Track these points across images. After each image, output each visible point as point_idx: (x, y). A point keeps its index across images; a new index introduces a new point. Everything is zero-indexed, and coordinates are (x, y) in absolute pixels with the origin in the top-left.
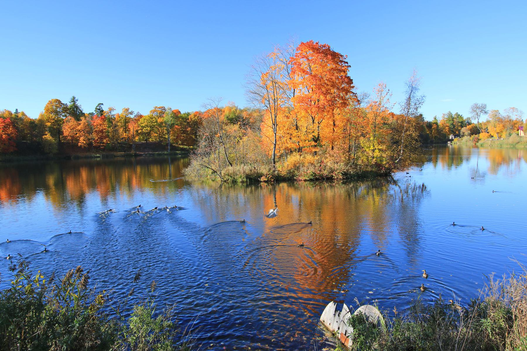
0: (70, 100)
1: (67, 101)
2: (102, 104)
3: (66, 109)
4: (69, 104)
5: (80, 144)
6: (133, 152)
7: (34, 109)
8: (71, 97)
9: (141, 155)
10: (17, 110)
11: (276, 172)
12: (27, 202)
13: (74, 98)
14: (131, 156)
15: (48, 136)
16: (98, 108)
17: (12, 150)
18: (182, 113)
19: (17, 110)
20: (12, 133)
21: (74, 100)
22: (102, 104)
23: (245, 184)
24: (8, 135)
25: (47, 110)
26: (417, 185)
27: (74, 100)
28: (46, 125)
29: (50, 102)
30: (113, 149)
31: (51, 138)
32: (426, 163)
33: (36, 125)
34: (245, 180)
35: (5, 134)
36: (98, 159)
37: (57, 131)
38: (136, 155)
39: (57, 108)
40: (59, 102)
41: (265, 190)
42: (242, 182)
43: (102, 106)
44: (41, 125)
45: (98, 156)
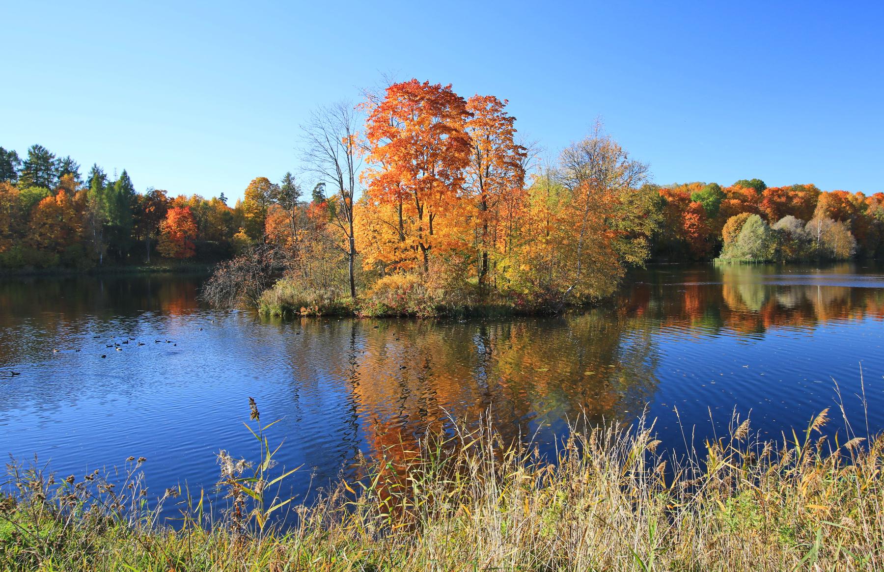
1: (277, 180)
2: (324, 184)
3: (275, 193)
7: (209, 195)
8: (285, 174)
10: (222, 194)
12: (859, 313)
13: (289, 175)
17: (188, 255)
18: (188, 197)
19: (222, 194)
20: (190, 230)
21: (289, 179)
22: (324, 184)
23: (279, 320)
24: (185, 232)
25: (248, 194)
27: (289, 179)
29: (254, 182)
32: (760, 276)
33: (232, 218)
35: (180, 231)
37: (257, 228)
39: (261, 190)
40: (265, 180)
42: (277, 315)
43: (324, 187)
44: (238, 217)
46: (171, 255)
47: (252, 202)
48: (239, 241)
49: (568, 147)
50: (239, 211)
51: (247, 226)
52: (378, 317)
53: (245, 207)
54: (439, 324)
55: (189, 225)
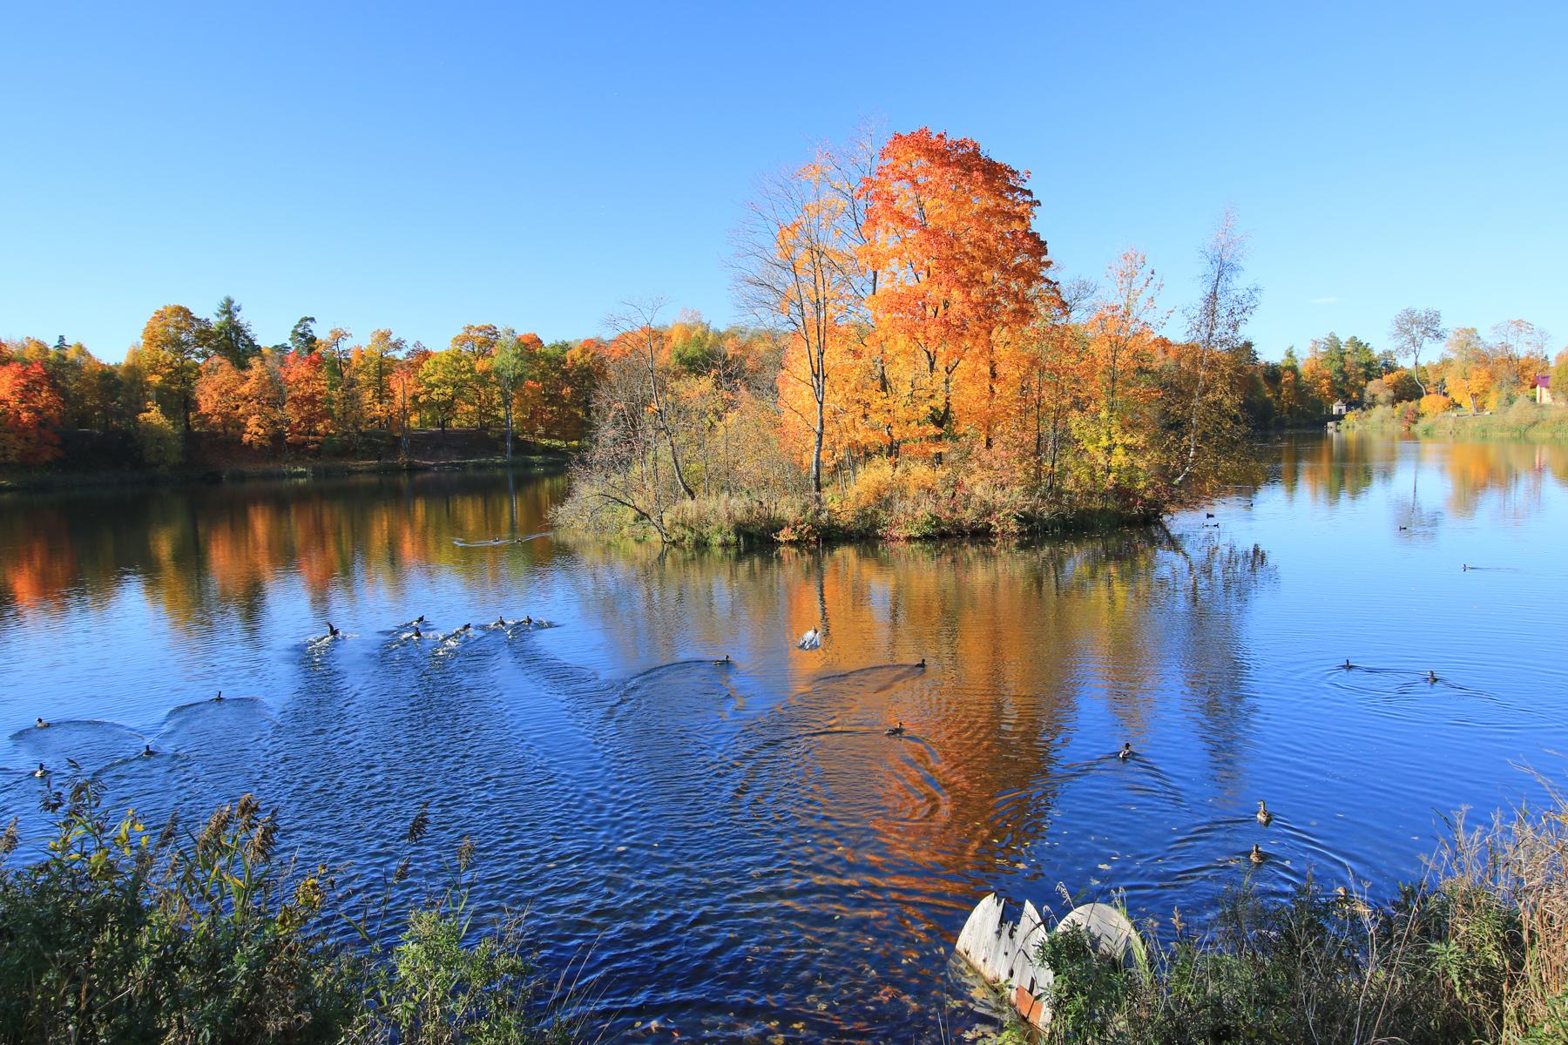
0: (216, 308)
1: (207, 311)
2: (312, 319)
3: (205, 335)
4: (215, 321)
5: (246, 437)
6: (402, 460)
8: (221, 299)
9: (426, 469)
10: (62, 338)
12: (1243, 501)
13: (230, 302)
14: (398, 470)
15: (154, 415)
16: (300, 330)
17: (48, 457)
19: (62, 338)
20: (48, 407)
21: (228, 309)
23: (732, 552)
24: (38, 411)
25: (151, 338)
27: (228, 309)
28: (148, 383)
29: (161, 316)
30: (346, 450)
31: (162, 420)
33: (119, 383)
35: (28, 409)
36: (301, 481)
37: (179, 400)
38: (412, 469)
39: (177, 329)
40: (187, 313)
41: (791, 566)
42: (725, 545)
43: (312, 326)
44: (134, 382)
45: (301, 473)
46: (11, 459)
47: (162, 353)
48: (149, 427)
49: (1344, 339)
50: (133, 370)
51: (160, 400)
52: (926, 538)
53: (145, 362)
54: (1022, 546)
55: (44, 397)
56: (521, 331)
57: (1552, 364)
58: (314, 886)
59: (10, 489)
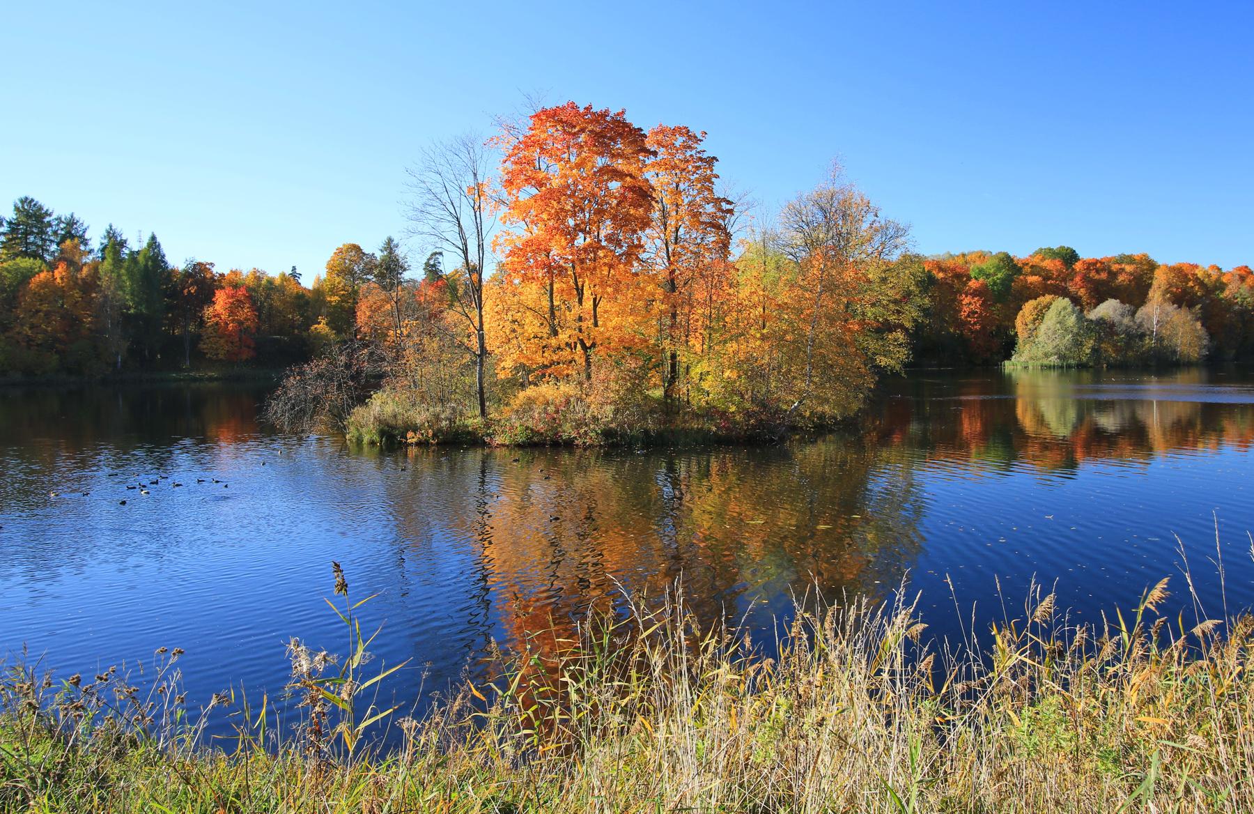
0: (381, 245)
1: (373, 247)
2: (441, 254)
7: (274, 270)
8: (385, 239)
10: (294, 268)
11: (970, 426)
12: (1213, 440)
13: (390, 240)
16: (432, 262)
17: (244, 357)
18: (245, 272)
19: (294, 268)
20: (246, 319)
21: (390, 246)
22: (441, 254)
23: (376, 450)
24: (240, 323)
25: (331, 268)
26: (491, 502)
27: (390, 246)
29: (340, 251)
31: (327, 329)
33: (307, 303)
34: (376, 438)
35: (233, 321)
39: (351, 263)
40: (357, 248)
41: (426, 468)
42: (372, 443)
44: (317, 301)
46: (221, 356)
48: (318, 336)
50: (318, 292)
52: (520, 446)
56: (1172, 262)
57: (32, 286)
58: (626, 764)
59: (216, 379)
